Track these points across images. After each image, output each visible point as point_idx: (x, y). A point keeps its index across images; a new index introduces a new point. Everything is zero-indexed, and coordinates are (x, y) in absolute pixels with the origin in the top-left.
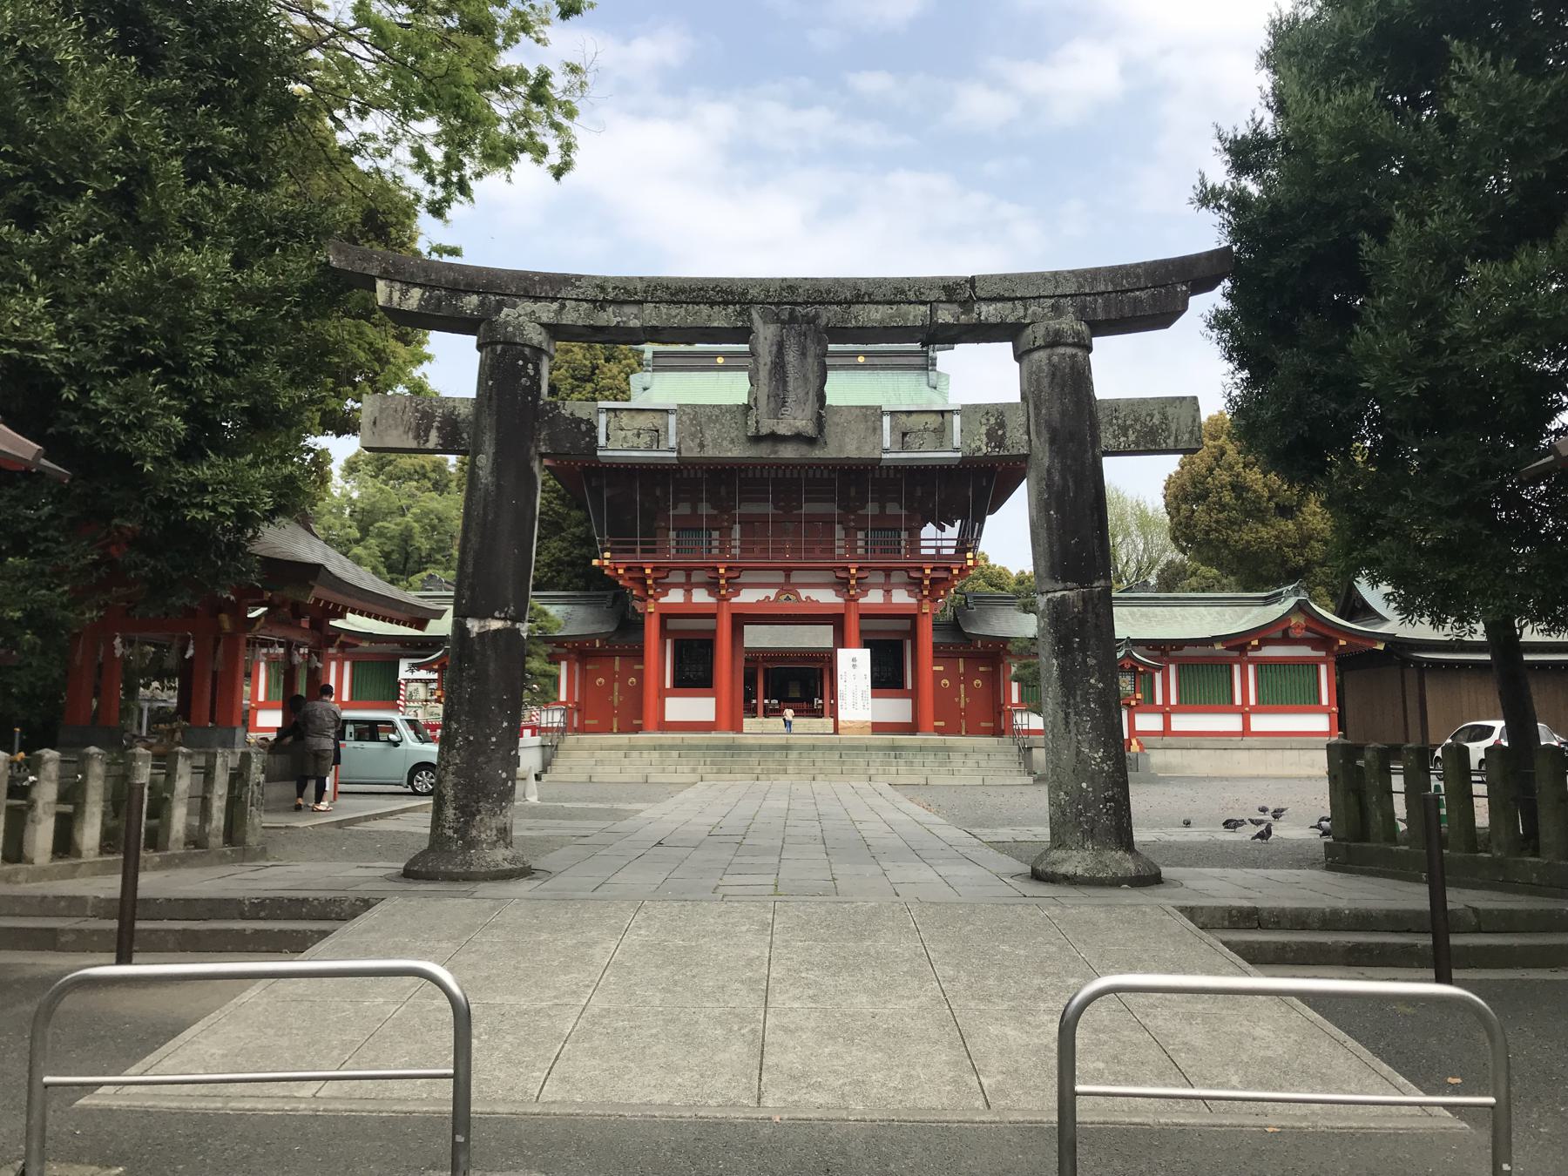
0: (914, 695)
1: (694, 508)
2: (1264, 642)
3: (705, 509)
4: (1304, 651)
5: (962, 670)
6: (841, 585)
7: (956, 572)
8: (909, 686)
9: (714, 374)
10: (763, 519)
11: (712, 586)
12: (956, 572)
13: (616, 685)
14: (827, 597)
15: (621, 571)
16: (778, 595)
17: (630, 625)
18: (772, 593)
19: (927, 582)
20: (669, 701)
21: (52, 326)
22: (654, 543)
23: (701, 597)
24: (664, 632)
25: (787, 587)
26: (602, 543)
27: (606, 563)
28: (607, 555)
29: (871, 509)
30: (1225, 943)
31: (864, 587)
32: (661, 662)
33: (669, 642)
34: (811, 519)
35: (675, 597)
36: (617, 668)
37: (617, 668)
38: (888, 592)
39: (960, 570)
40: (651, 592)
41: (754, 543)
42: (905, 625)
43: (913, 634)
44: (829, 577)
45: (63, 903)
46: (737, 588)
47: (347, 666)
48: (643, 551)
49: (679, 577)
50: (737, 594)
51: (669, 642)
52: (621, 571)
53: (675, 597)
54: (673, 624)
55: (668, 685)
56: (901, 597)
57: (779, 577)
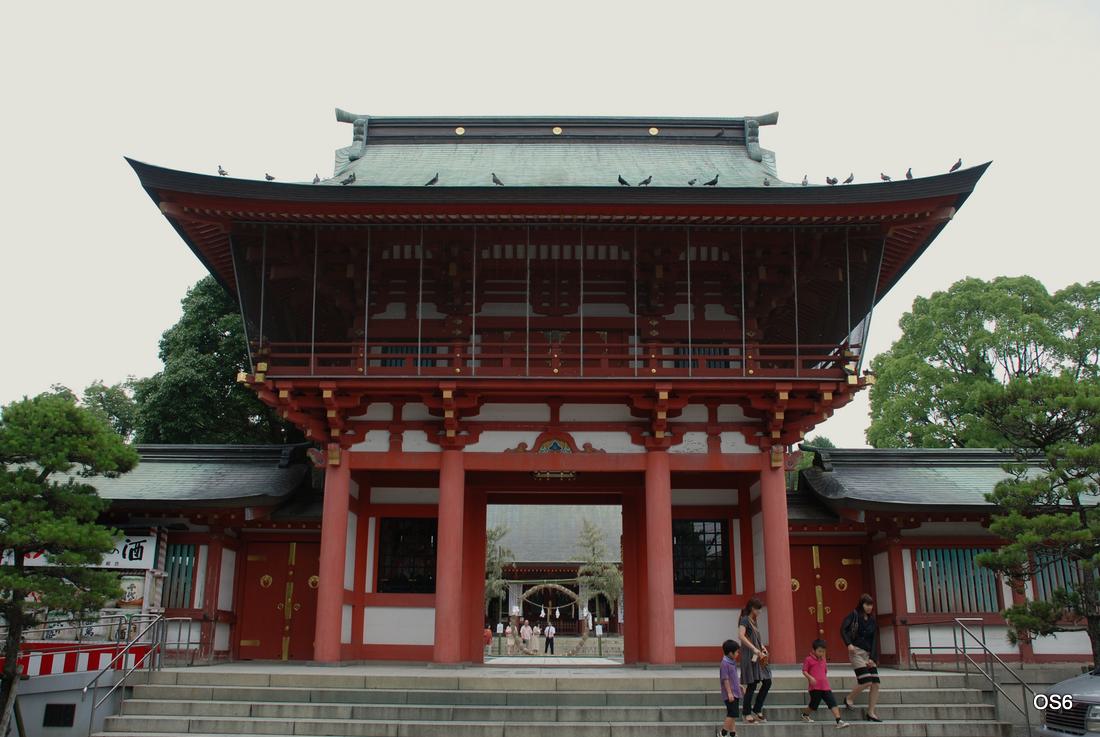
0: (750, 605)
1: (411, 310)
2: (1022, 593)
3: (425, 311)
4: (1082, 581)
5: (816, 564)
6: (642, 428)
7: (828, 396)
8: (739, 589)
9: (449, 147)
10: (516, 325)
11: (433, 429)
12: (828, 396)
13: (290, 587)
14: (617, 445)
15: (284, 394)
16: (539, 442)
17: (305, 493)
18: (530, 438)
19: (780, 416)
20: (371, 614)
21: (725, 658)
22: (348, 350)
23: (415, 443)
24: (360, 506)
25: (555, 430)
26: (254, 349)
27: (259, 378)
28: (263, 366)
29: (685, 312)
30: (564, 585)
31: (677, 433)
32: (343, 550)
33: (372, 522)
34: (593, 326)
35: (376, 442)
36: (292, 560)
37: (292, 560)
38: (714, 441)
39: (835, 394)
40: (335, 433)
41: (501, 350)
42: (728, 497)
43: (749, 508)
44: (620, 412)
45: (988, 375)
46: (475, 431)
47: (228, 558)
48: (322, 362)
49: (380, 411)
50: (474, 439)
51: (372, 522)
52: (284, 394)
53: (376, 442)
54: (381, 495)
55: (369, 588)
56: (734, 444)
57: (540, 412)
